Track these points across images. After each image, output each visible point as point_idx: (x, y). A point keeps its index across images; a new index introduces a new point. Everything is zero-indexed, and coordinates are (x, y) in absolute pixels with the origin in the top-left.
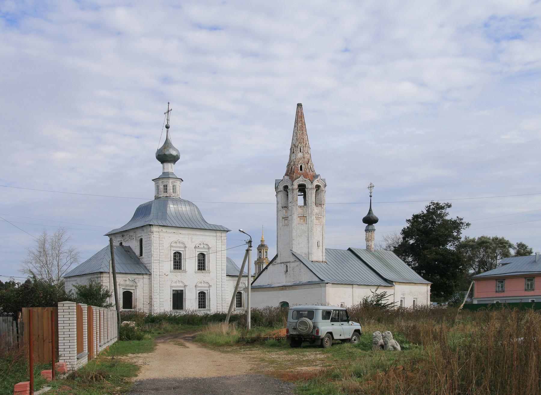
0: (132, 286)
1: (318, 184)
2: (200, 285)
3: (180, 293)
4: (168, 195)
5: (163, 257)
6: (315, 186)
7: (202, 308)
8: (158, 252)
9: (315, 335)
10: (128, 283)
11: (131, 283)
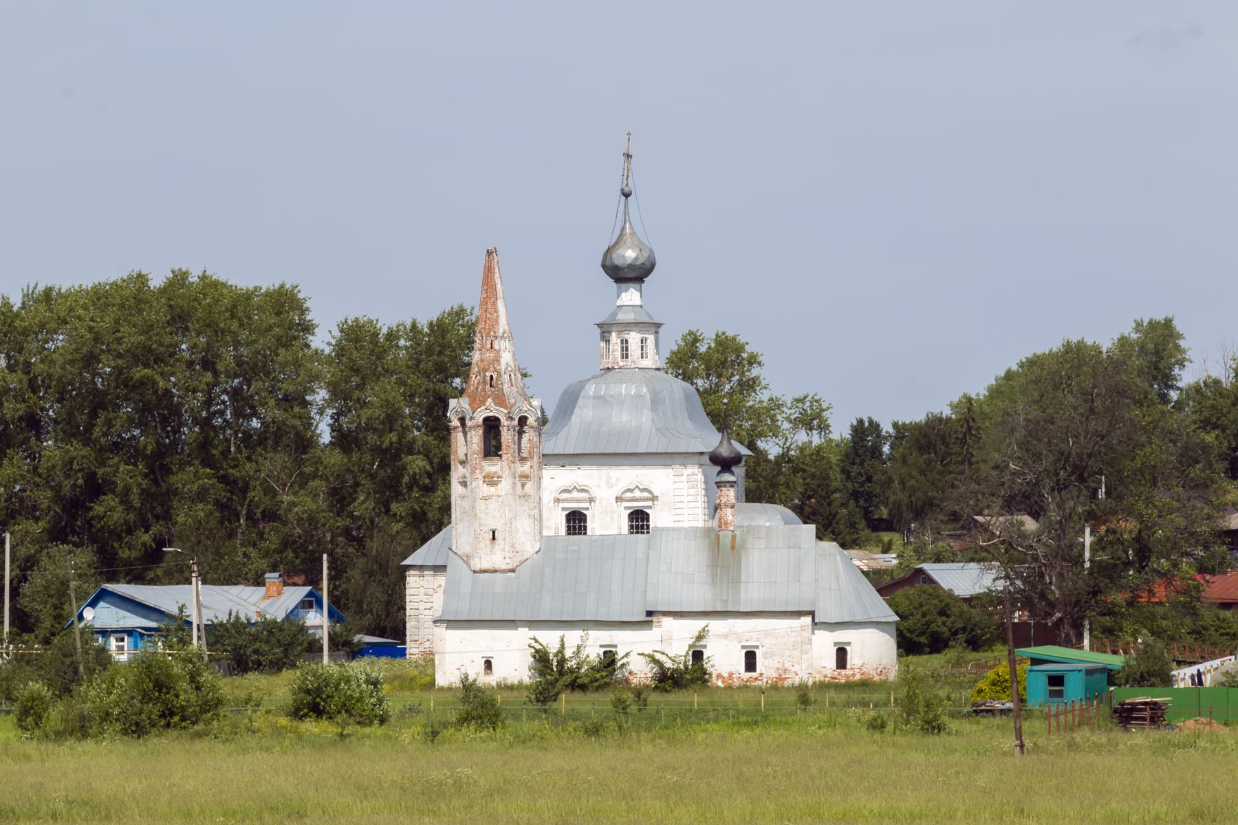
1: (491, 414)
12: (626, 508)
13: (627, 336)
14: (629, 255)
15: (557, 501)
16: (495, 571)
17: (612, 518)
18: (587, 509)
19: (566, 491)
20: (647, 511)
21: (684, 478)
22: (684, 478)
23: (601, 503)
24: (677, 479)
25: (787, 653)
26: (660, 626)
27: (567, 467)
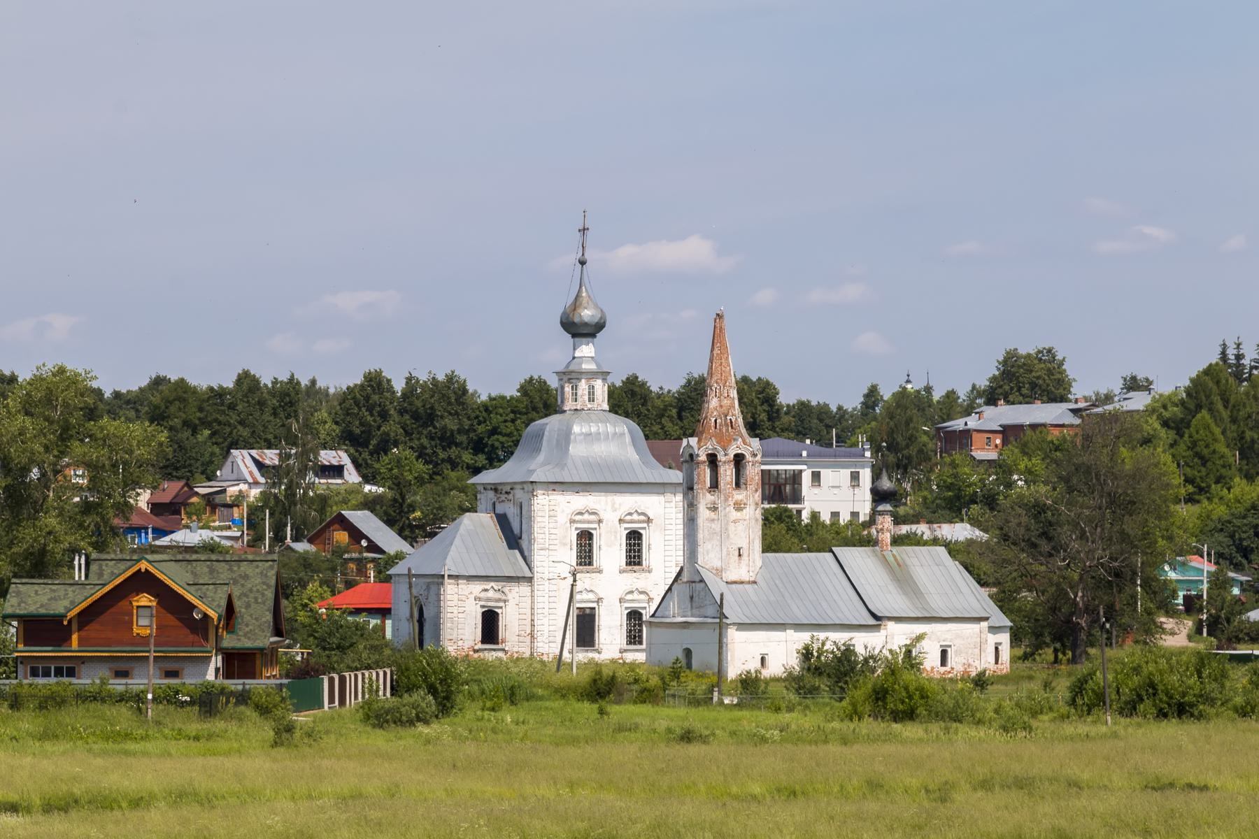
0: (499, 600)
1: (739, 452)
2: (629, 597)
3: (589, 615)
4: (578, 408)
5: (556, 542)
6: (732, 456)
7: (635, 643)
8: (547, 533)
9: (378, 670)
10: (491, 594)
11: (498, 595)
12: (626, 529)
13: (593, 383)
14: (587, 314)
15: (572, 522)
16: (742, 583)
17: (616, 537)
18: (645, 528)
19: (581, 513)
20: (641, 531)
21: (673, 504)
22: (673, 504)
23: (607, 524)
24: (667, 505)
25: (970, 651)
26: (886, 629)
27: (581, 494)
